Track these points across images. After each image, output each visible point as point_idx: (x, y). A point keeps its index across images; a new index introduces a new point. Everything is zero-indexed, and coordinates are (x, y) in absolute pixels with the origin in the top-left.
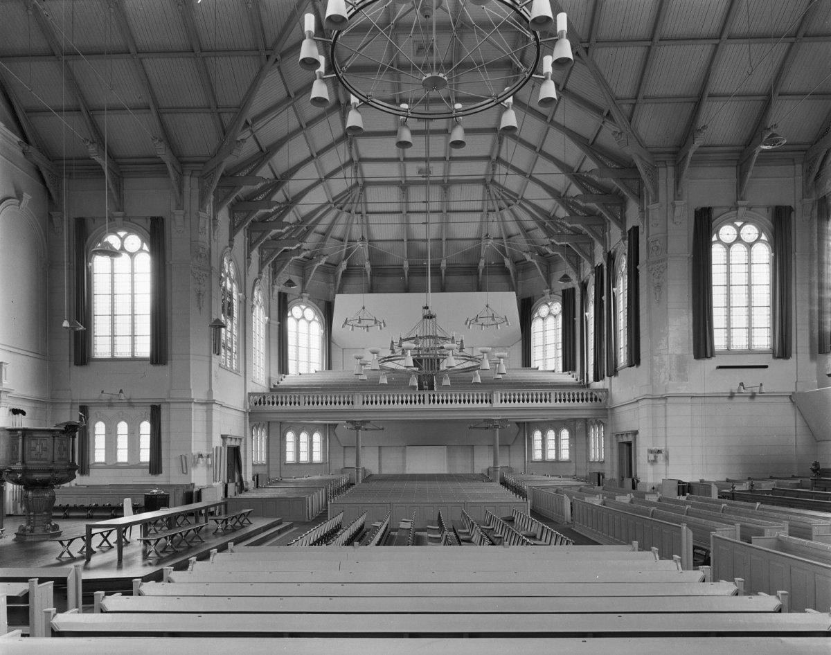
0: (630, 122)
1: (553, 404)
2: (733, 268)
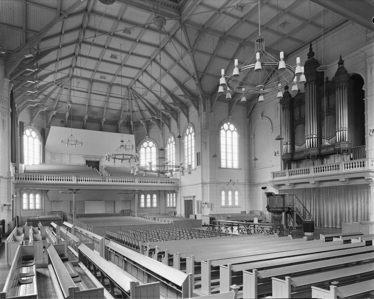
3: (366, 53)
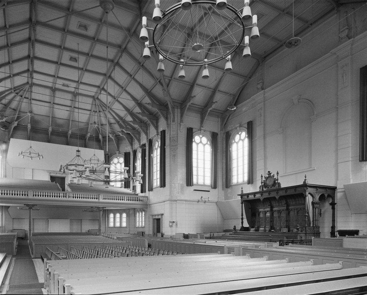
0: (168, 87)
1: (125, 202)
2: (199, 152)
3: (338, 56)
